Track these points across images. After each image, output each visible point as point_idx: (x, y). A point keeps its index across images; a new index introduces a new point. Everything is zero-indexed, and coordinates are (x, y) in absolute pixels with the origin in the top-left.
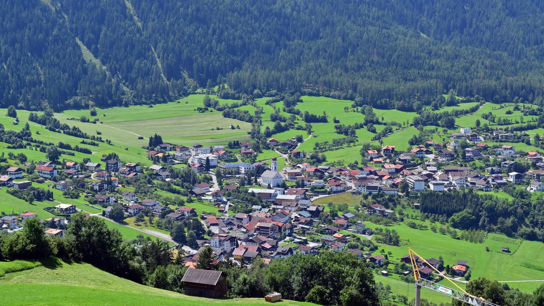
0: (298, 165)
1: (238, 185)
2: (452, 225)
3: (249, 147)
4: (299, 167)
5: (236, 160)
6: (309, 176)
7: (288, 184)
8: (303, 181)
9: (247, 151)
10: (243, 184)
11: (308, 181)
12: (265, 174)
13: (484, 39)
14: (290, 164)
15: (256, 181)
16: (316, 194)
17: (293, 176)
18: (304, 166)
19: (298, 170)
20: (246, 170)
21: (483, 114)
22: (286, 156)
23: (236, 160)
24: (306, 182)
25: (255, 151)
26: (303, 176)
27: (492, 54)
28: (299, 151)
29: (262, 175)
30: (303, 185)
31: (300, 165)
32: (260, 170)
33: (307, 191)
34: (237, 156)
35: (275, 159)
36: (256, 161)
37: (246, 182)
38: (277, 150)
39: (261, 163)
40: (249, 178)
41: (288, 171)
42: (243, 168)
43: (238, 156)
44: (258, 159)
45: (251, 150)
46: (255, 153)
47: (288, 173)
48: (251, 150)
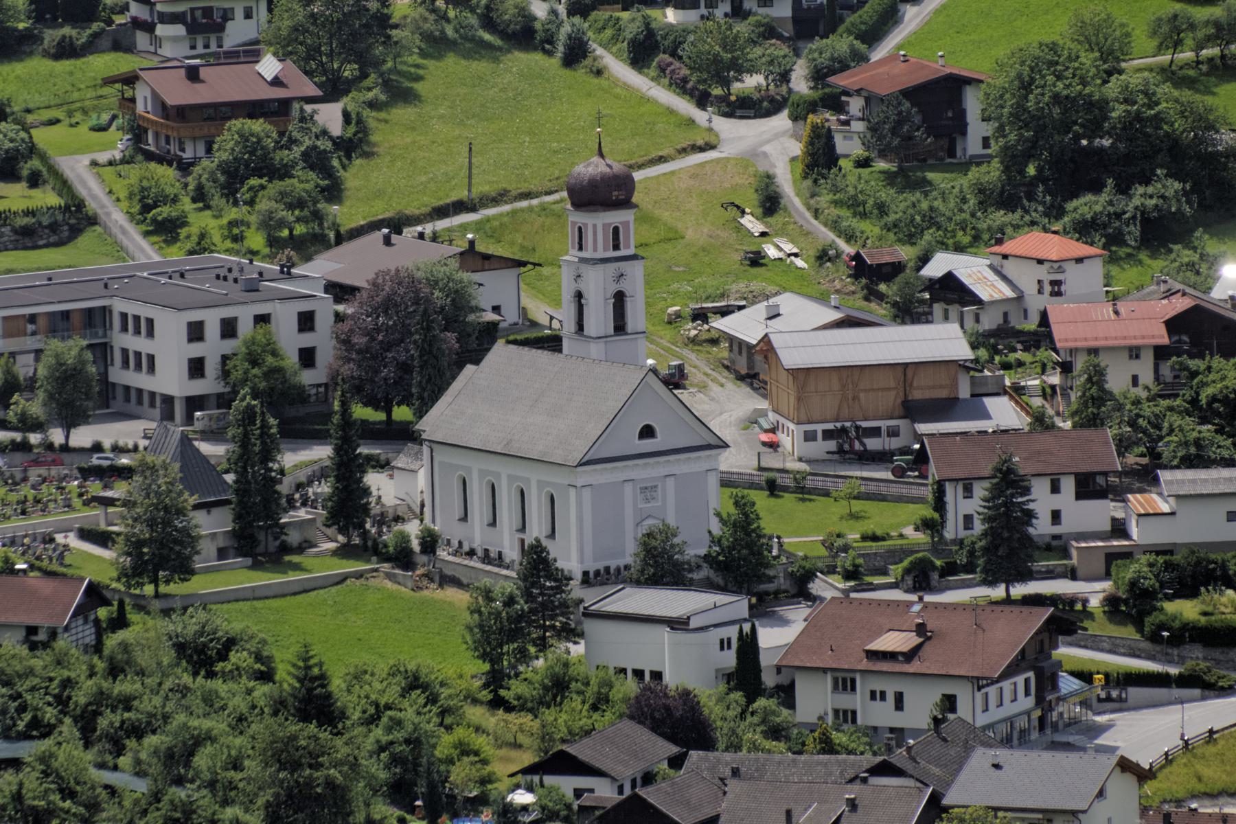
0: (938, 266)
1: (101, 563)
2: (823, 749)
3: (237, 32)
4: (951, 291)
5: (73, 220)
6: (1095, 407)
7: (795, 532)
8: (1009, 483)
9: (223, 85)
10: (161, 553)
11: (1088, 487)
12: (478, 405)
13: (231, 704)
14: (824, 257)
15: (349, 506)
16: (1196, 658)
17: (870, 424)
18: (1028, 277)
19: (942, 340)
20: (212, 348)
21: (669, 533)
22: (775, 142)
23: (73, 220)
24: (1053, 508)
25: (334, 90)
26: (1003, 413)
27: (143, 756)
28: (940, 61)
29: (434, 423)
30: (1009, 548)
31: (973, 270)
32: (418, 347)
33: (1065, 620)
34: (77, 168)
35: (605, 194)
36: (345, 214)
37: (211, 526)
38: (643, 51)
39: (414, 255)
40: (255, 456)
41: (792, 355)
42: (171, 326)
43: (88, 162)
44: (366, 190)
45: (269, 66)
46: (330, 116)
47: (803, 375)
48: (269, 66)
